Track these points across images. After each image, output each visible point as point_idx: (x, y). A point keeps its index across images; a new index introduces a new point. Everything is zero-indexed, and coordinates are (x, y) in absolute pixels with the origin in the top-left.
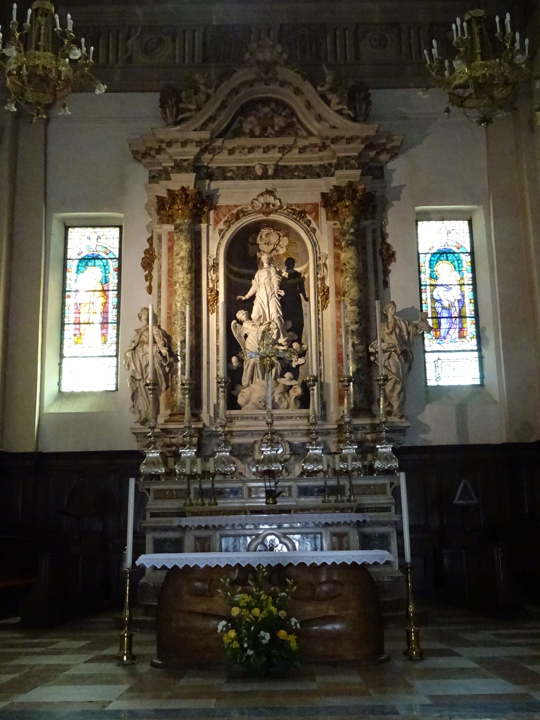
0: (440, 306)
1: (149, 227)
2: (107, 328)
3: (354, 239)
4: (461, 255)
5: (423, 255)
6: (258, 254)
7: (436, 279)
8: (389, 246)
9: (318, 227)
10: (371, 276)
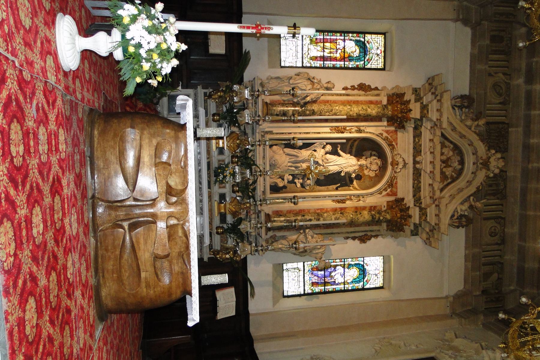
1: (384, 88)
2: (320, 61)
3: (376, 220)
4: (362, 283)
5: (362, 260)
6: (364, 157)
7: (348, 268)
8: (370, 239)
9: (383, 196)
10: (352, 229)
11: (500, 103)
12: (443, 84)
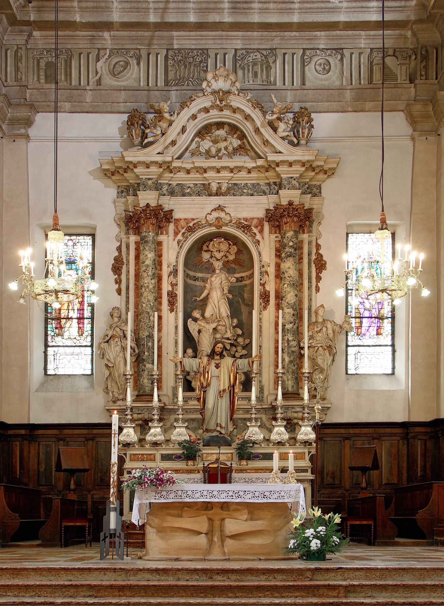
0: (363, 307)
2: (83, 323)
8: (322, 256)
11: (138, 64)
12: (113, 158)
